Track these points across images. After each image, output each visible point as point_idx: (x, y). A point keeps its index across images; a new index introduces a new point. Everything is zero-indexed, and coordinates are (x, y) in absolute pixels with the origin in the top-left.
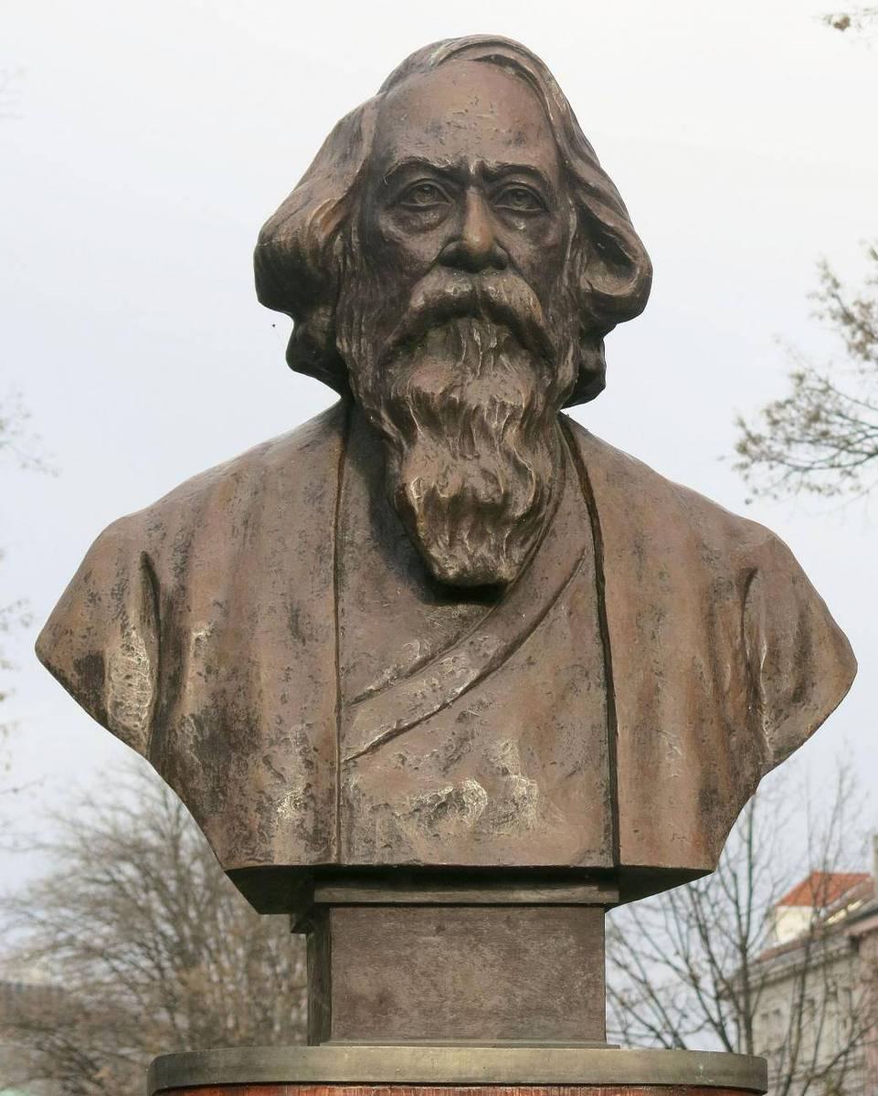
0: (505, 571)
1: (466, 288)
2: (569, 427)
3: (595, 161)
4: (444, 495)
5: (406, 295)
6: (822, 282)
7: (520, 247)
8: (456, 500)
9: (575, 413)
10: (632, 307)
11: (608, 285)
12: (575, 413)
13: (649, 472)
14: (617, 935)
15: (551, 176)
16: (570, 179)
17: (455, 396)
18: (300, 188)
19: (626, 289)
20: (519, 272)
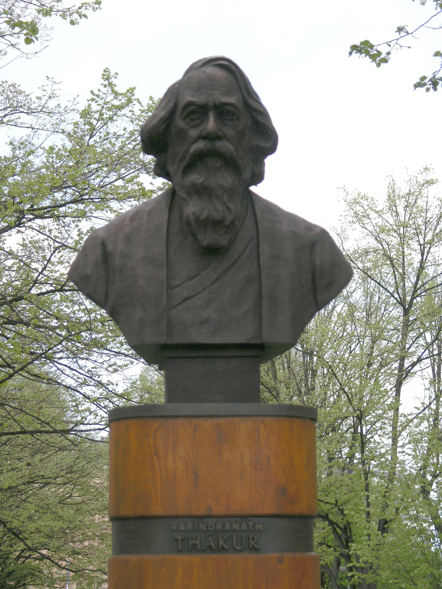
0: (224, 242)
1: (209, 146)
2: (251, 194)
3: (258, 99)
4: (202, 218)
5: (189, 149)
6: (4, 156)
7: (229, 132)
8: (207, 219)
9: (253, 188)
10: (272, 149)
11: (263, 144)
12: (253, 188)
13: (279, 208)
14: (6, 37)
15: (240, 106)
16: (247, 105)
17: (206, 183)
18: (187, 76)
19: (269, 145)
20: (228, 140)
